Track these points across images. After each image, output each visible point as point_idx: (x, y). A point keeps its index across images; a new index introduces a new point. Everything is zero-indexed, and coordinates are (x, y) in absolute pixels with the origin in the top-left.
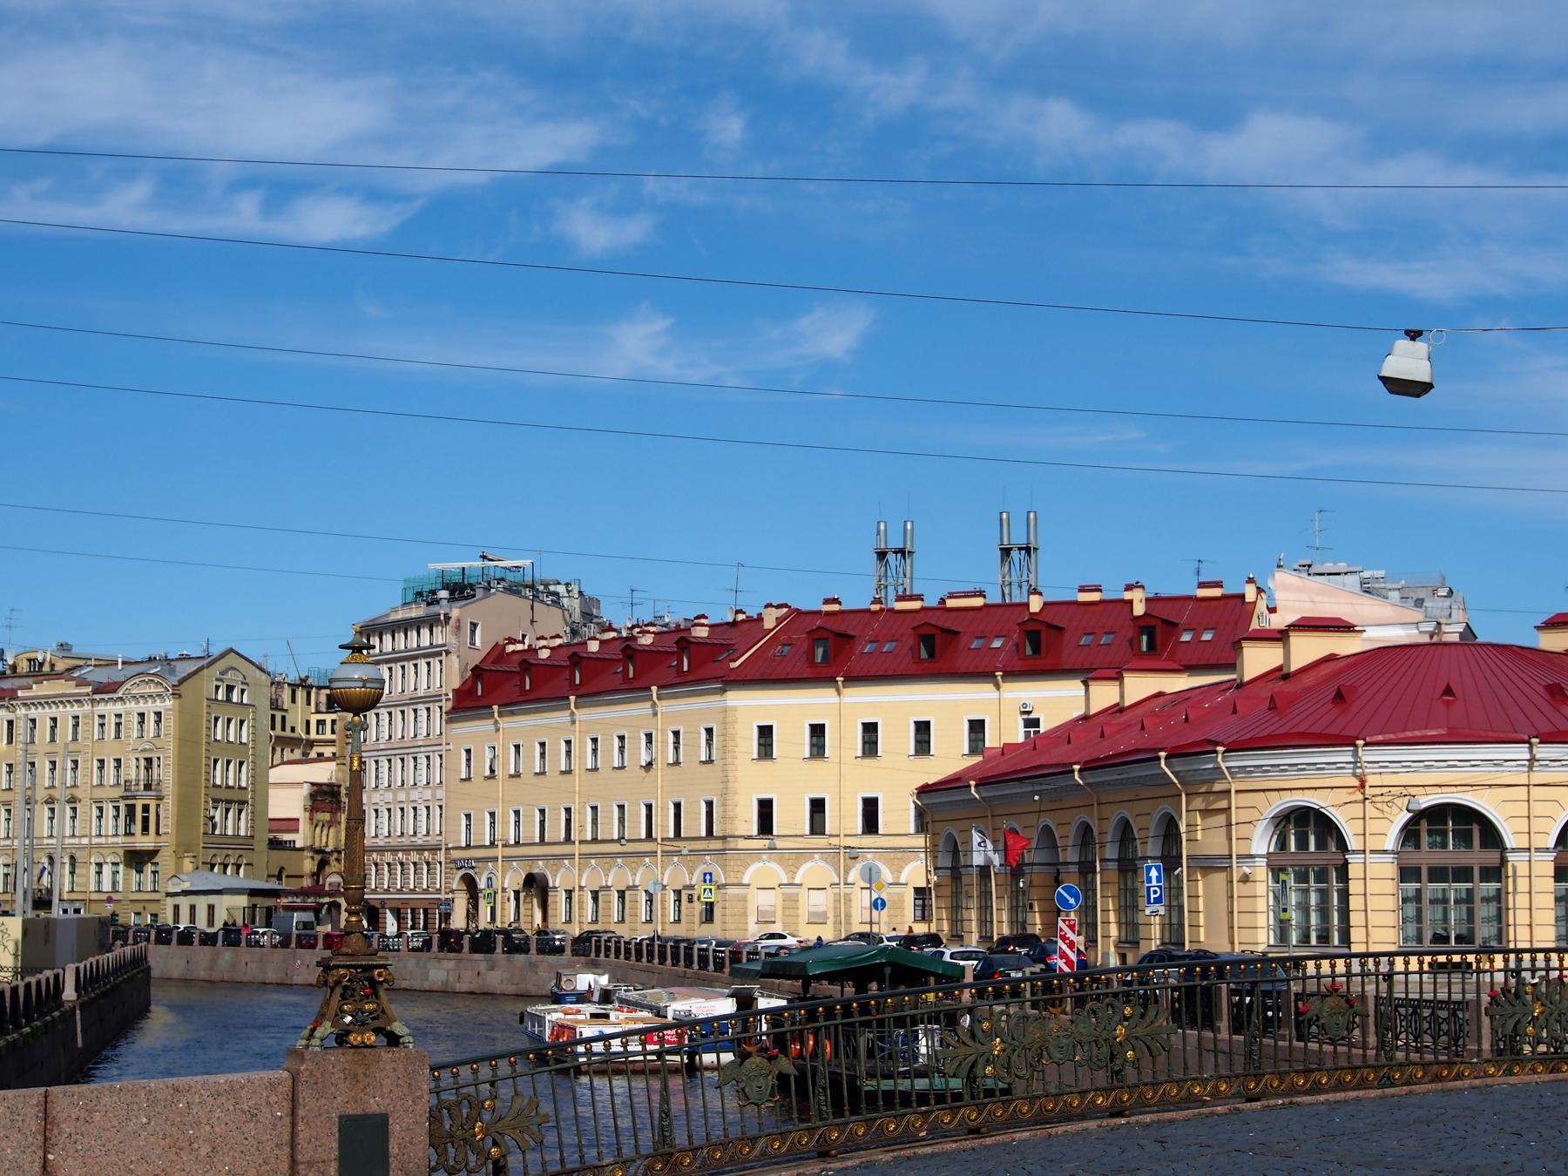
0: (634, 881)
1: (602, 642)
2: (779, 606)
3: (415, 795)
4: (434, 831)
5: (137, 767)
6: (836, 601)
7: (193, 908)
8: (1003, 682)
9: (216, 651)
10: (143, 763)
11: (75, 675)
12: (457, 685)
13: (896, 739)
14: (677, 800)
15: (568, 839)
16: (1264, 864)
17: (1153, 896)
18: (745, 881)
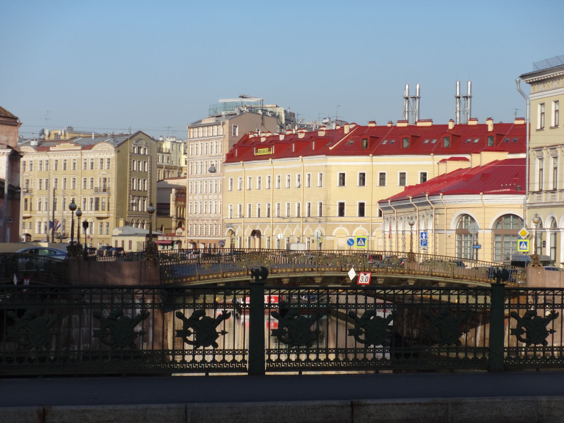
0: (313, 234)
1: (286, 136)
2: (352, 124)
3: (211, 197)
4: (218, 212)
5: (100, 181)
6: (374, 122)
7: (130, 242)
8: (4, 180)
9: (133, 132)
10: (102, 180)
11: (74, 141)
12: (227, 152)
13: (372, 180)
14: (309, 202)
15: (299, 217)
16: (455, 233)
17: (423, 243)
18: (333, 235)
